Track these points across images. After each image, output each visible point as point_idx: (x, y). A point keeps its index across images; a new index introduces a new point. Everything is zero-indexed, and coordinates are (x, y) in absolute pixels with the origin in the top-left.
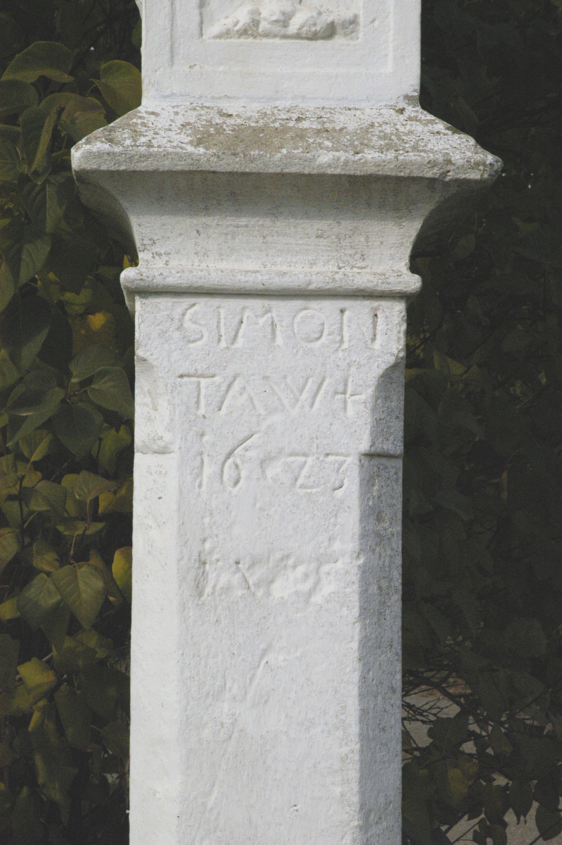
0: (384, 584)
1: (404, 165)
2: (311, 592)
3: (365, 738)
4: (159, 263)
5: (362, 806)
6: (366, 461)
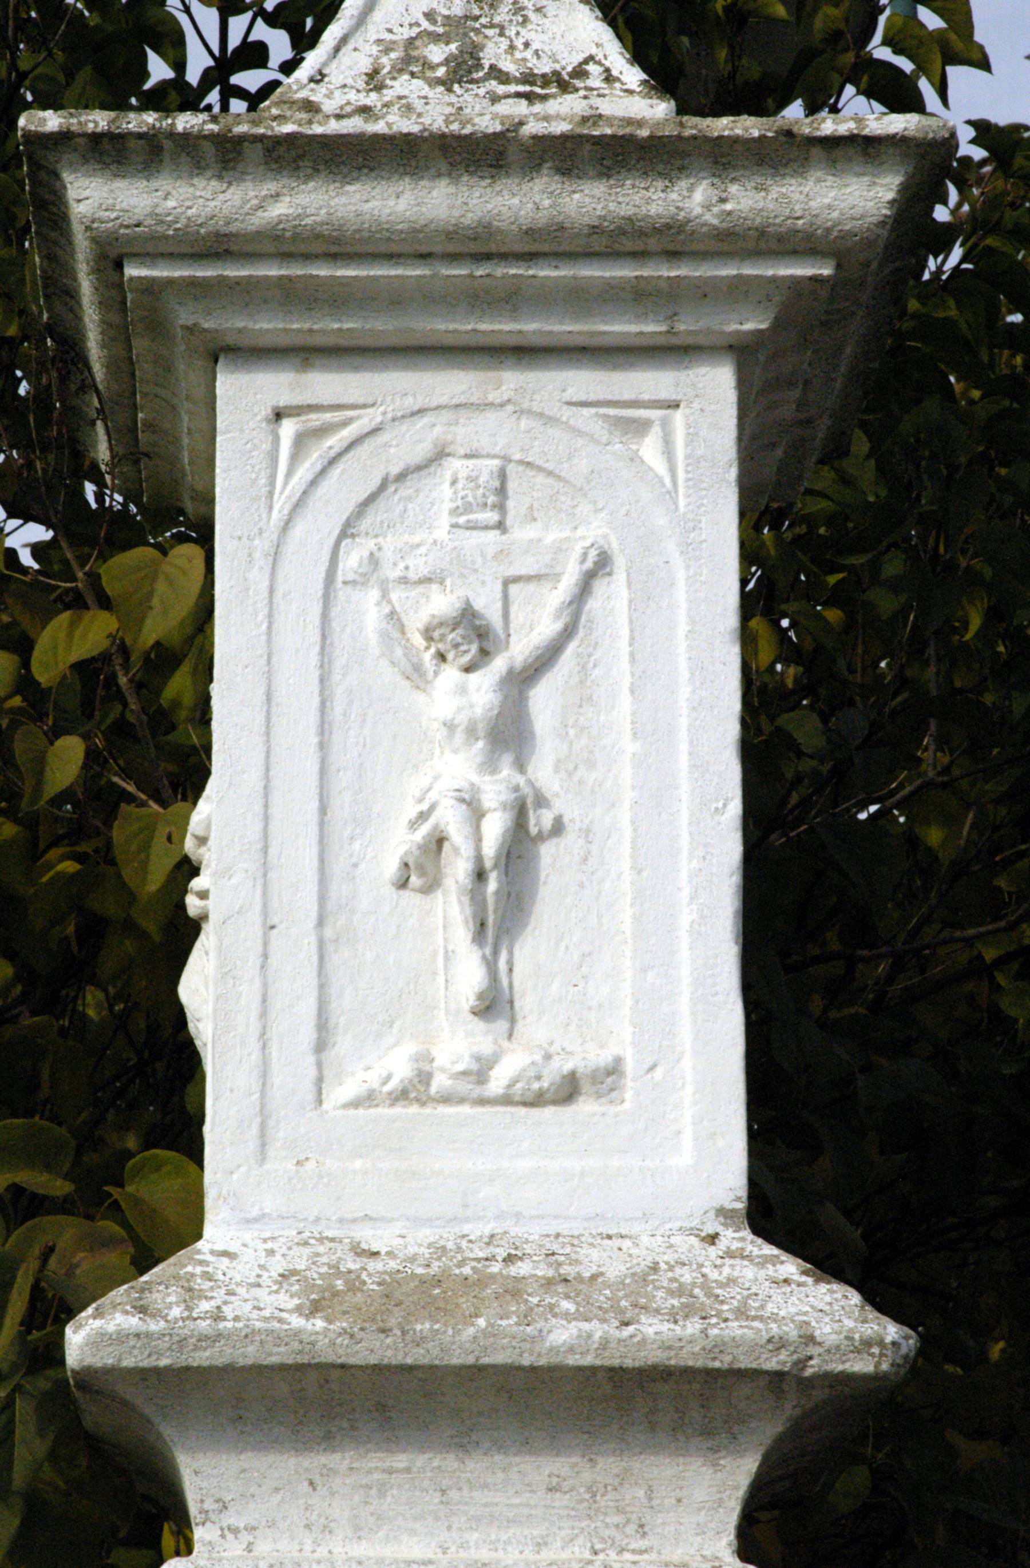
1: (719, 1347)
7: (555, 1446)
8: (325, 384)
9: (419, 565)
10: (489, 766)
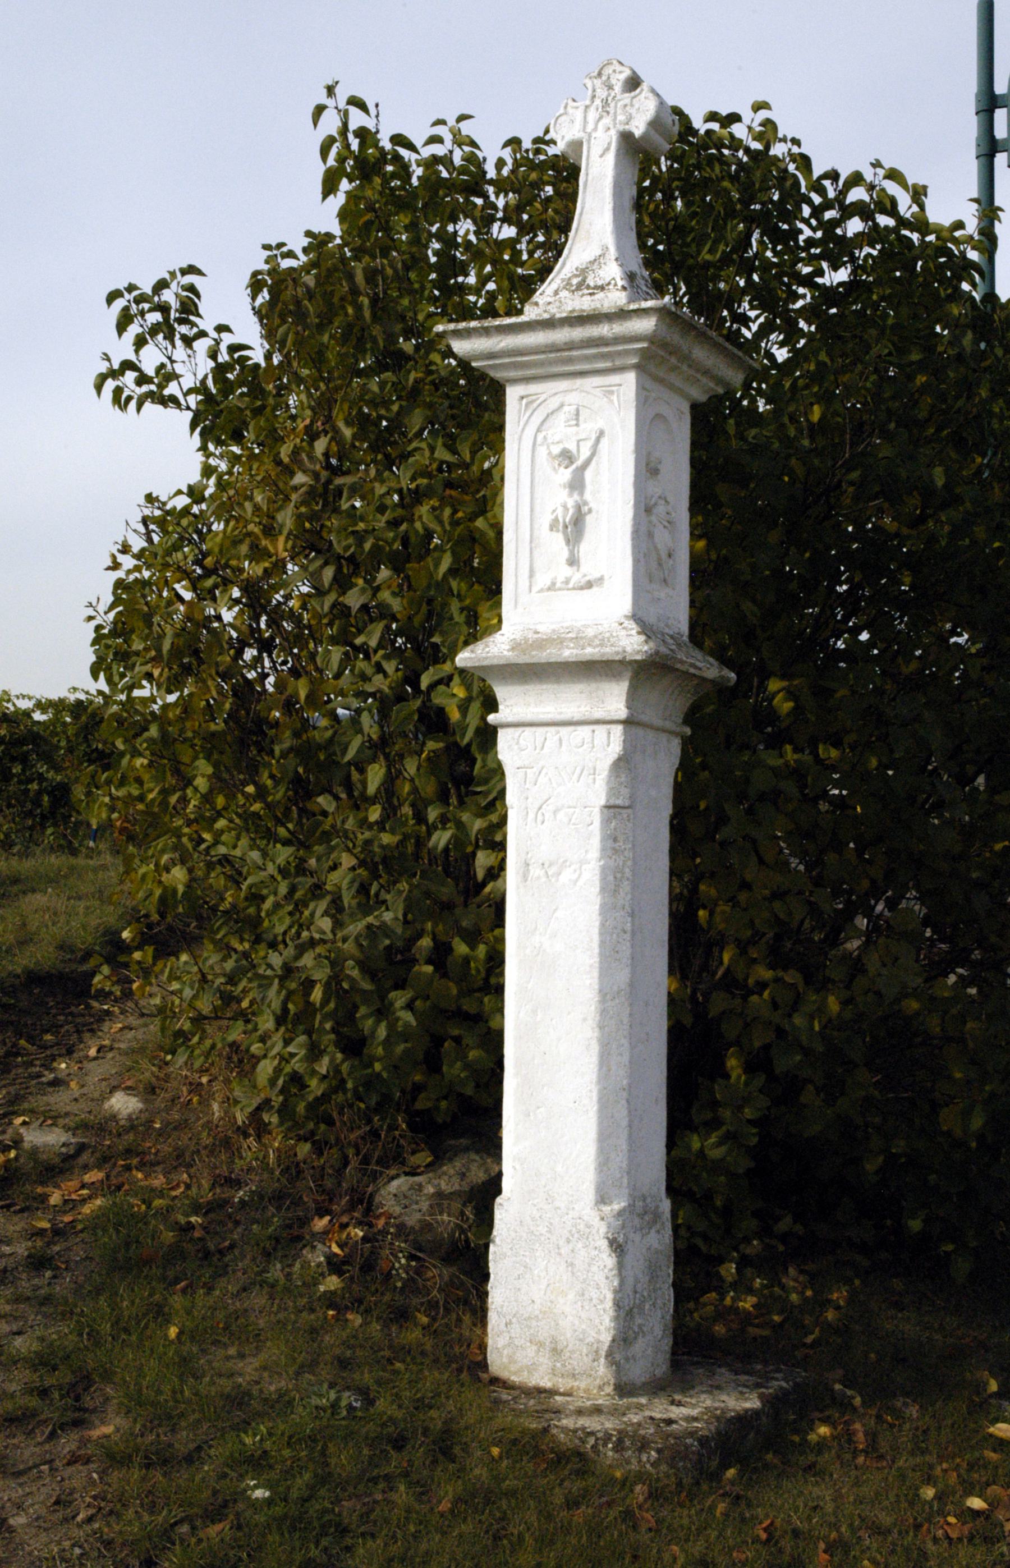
0: (619, 875)
1: (603, 654)
2: (577, 880)
3: (602, 955)
4: (508, 711)
5: (600, 991)
6: (605, 811)
7: (580, 681)
8: (533, 388)
9: (557, 439)
10: (571, 495)
